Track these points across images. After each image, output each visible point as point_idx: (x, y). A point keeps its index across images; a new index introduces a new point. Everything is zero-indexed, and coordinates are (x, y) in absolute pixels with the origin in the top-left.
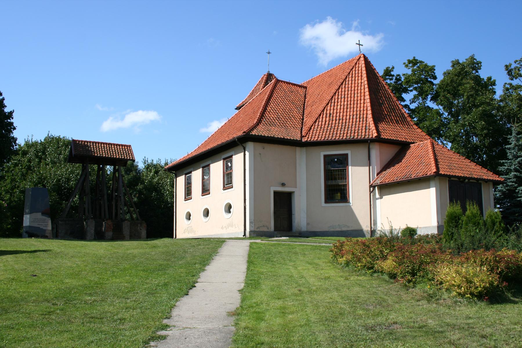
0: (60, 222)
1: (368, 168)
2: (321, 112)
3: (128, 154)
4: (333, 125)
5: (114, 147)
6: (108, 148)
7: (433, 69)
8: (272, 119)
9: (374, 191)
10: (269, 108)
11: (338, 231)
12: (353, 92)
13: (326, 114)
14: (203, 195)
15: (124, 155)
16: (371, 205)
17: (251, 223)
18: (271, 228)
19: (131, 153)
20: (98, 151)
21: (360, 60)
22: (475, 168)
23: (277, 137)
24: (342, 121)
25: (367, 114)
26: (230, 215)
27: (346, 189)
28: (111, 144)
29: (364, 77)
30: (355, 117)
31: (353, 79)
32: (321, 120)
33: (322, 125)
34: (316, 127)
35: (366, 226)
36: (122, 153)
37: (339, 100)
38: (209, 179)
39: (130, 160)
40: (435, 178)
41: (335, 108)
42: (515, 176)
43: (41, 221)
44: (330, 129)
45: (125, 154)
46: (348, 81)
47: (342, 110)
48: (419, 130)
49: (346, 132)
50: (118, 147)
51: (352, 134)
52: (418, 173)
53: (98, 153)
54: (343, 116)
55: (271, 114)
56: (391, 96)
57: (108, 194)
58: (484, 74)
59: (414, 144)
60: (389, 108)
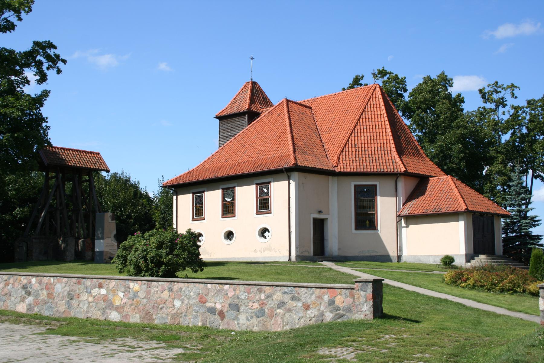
7: (403, 81)
12: (374, 123)
14: (224, 216)
30: (379, 149)
35: (392, 252)
47: (366, 142)
48: (432, 163)
52: (448, 207)
56: (405, 128)
58: (453, 91)
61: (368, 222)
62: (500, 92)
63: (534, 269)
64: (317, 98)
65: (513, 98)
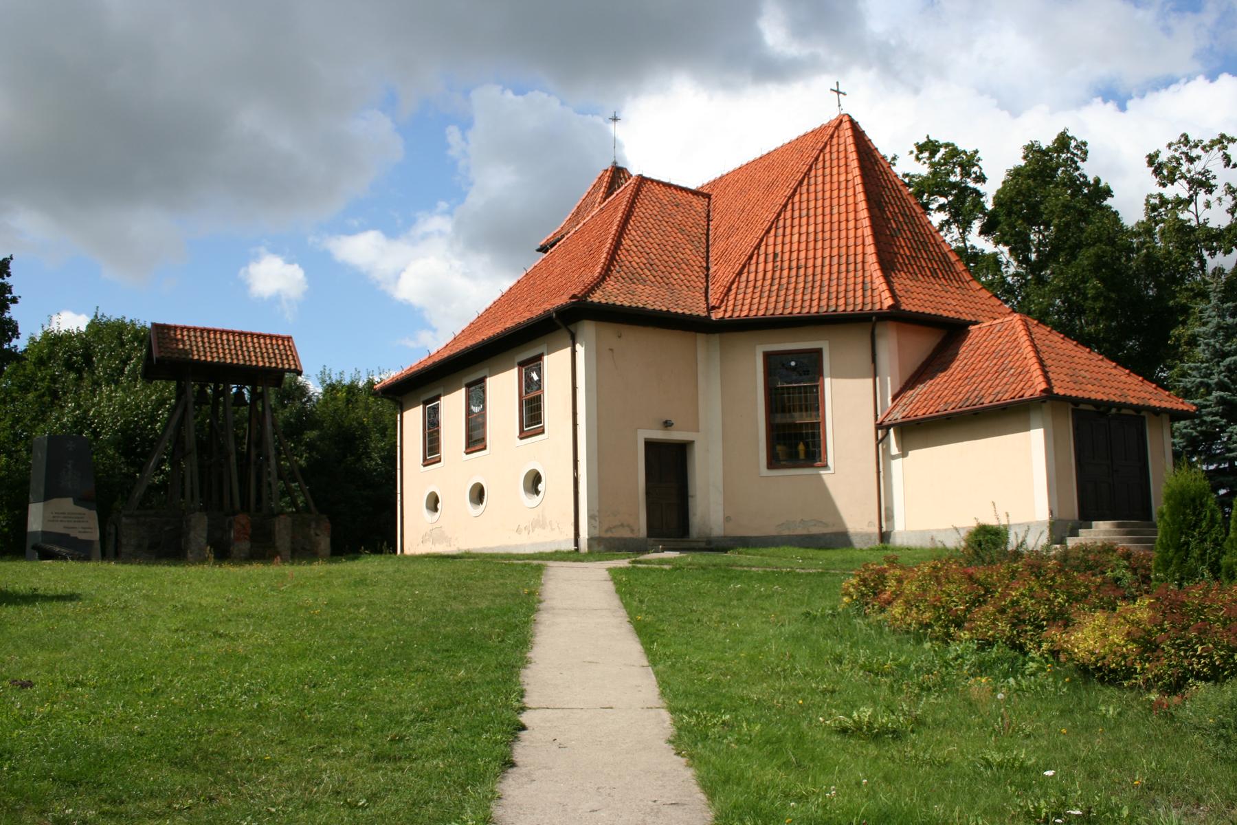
0: (124, 520)
1: (870, 381)
2: (754, 251)
3: (284, 357)
4: (784, 281)
5: (253, 342)
6: (238, 343)
8: (636, 266)
9: (885, 440)
10: (628, 241)
11: (801, 536)
12: (827, 203)
13: (766, 255)
15: (276, 359)
16: (878, 472)
17: (591, 517)
18: (639, 530)
19: (292, 355)
20: (214, 350)
21: (841, 128)
22: (1129, 380)
23: (652, 308)
24: (805, 271)
25: (864, 254)
27: (819, 433)
28: (246, 334)
29: (853, 166)
30: (835, 260)
31: (827, 171)
32: (753, 268)
33: (756, 281)
34: (743, 285)
36: (272, 355)
37: (796, 222)
38: (483, 412)
39: (289, 370)
40: (1044, 405)
41: (787, 239)
42: (1221, 401)
43: (73, 520)
44: (778, 290)
45: (278, 357)
46: (816, 176)
47: (803, 246)
49: (815, 296)
50: (262, 341)
51: (833, 302)
52: (999, 393)
53: (215, 355)
54: (806, 259)
55: (633, 254)
57: (239, 454)
59: (978, 326)
60: (915, 241)
62: (1199, 157)
63: (1171, 554)
65: (1228, 169)
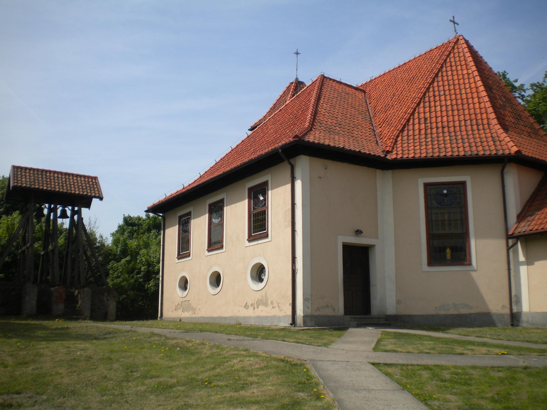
14: (210, 249)
16: (509, 270)
17: (305, 300)
21: (459, 43)
26: (262, 285)
38: (221, 224)
61: (448, 251)
64: (374, 78)
